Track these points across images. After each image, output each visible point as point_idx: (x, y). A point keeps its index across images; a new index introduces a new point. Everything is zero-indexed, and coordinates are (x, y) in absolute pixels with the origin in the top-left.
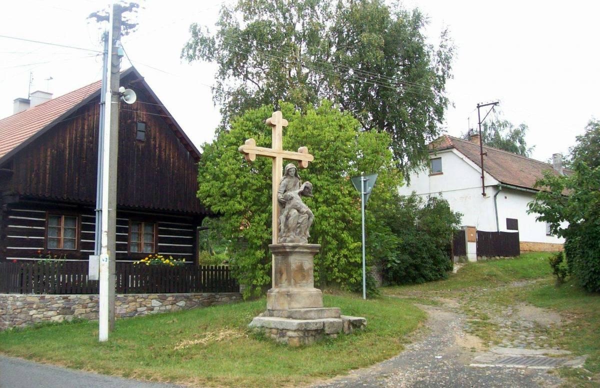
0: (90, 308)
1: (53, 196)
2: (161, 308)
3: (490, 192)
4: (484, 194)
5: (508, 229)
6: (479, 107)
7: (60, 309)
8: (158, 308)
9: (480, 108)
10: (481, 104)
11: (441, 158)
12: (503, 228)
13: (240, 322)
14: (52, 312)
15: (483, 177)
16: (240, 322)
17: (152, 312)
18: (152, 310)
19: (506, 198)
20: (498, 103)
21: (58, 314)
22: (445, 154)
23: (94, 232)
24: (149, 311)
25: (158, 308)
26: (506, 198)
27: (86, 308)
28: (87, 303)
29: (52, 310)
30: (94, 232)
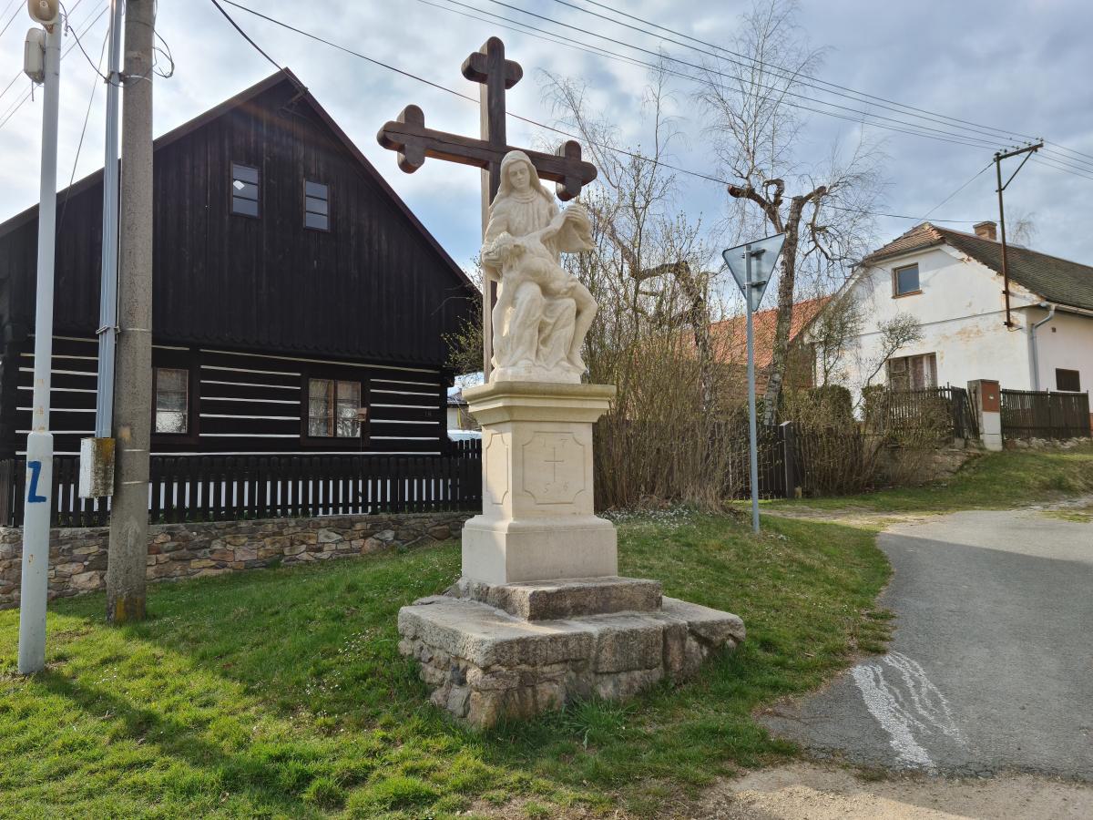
0: (167, 552)
1: (169, 374)
2: (340, 547)
3: (1021, 319)
4: (1009, 324)
5: (1058, 388)
6: (999, 158)
7: (90, 558)
8: (334, 546)
9: (1001, 162)
10: (1003, 153)
11: (917, 264)
12: (1049, 385)
13: (994, 491)
14: (74, 565)
15: (1007, 293)
16: (994, 491)
17: (318, 555)
18: (320, 550)
19: (1054, 330)
20: (1041, 146)
21: (87, 569)
22: (925, 255)
23: (30, 388)
24: (312, 553)
25: (334, 546)
26: (1054, 330)
27: (159, 553)
28: (162, 543)
29: (73, 562)
30: (30, 388)
